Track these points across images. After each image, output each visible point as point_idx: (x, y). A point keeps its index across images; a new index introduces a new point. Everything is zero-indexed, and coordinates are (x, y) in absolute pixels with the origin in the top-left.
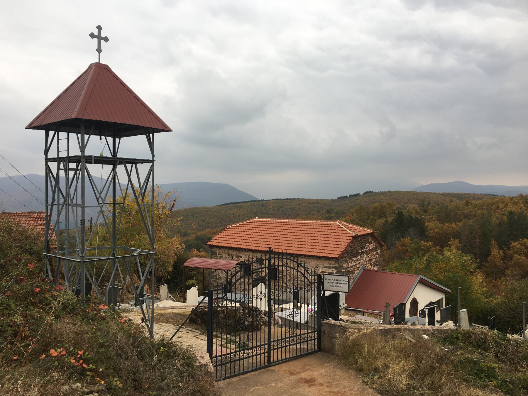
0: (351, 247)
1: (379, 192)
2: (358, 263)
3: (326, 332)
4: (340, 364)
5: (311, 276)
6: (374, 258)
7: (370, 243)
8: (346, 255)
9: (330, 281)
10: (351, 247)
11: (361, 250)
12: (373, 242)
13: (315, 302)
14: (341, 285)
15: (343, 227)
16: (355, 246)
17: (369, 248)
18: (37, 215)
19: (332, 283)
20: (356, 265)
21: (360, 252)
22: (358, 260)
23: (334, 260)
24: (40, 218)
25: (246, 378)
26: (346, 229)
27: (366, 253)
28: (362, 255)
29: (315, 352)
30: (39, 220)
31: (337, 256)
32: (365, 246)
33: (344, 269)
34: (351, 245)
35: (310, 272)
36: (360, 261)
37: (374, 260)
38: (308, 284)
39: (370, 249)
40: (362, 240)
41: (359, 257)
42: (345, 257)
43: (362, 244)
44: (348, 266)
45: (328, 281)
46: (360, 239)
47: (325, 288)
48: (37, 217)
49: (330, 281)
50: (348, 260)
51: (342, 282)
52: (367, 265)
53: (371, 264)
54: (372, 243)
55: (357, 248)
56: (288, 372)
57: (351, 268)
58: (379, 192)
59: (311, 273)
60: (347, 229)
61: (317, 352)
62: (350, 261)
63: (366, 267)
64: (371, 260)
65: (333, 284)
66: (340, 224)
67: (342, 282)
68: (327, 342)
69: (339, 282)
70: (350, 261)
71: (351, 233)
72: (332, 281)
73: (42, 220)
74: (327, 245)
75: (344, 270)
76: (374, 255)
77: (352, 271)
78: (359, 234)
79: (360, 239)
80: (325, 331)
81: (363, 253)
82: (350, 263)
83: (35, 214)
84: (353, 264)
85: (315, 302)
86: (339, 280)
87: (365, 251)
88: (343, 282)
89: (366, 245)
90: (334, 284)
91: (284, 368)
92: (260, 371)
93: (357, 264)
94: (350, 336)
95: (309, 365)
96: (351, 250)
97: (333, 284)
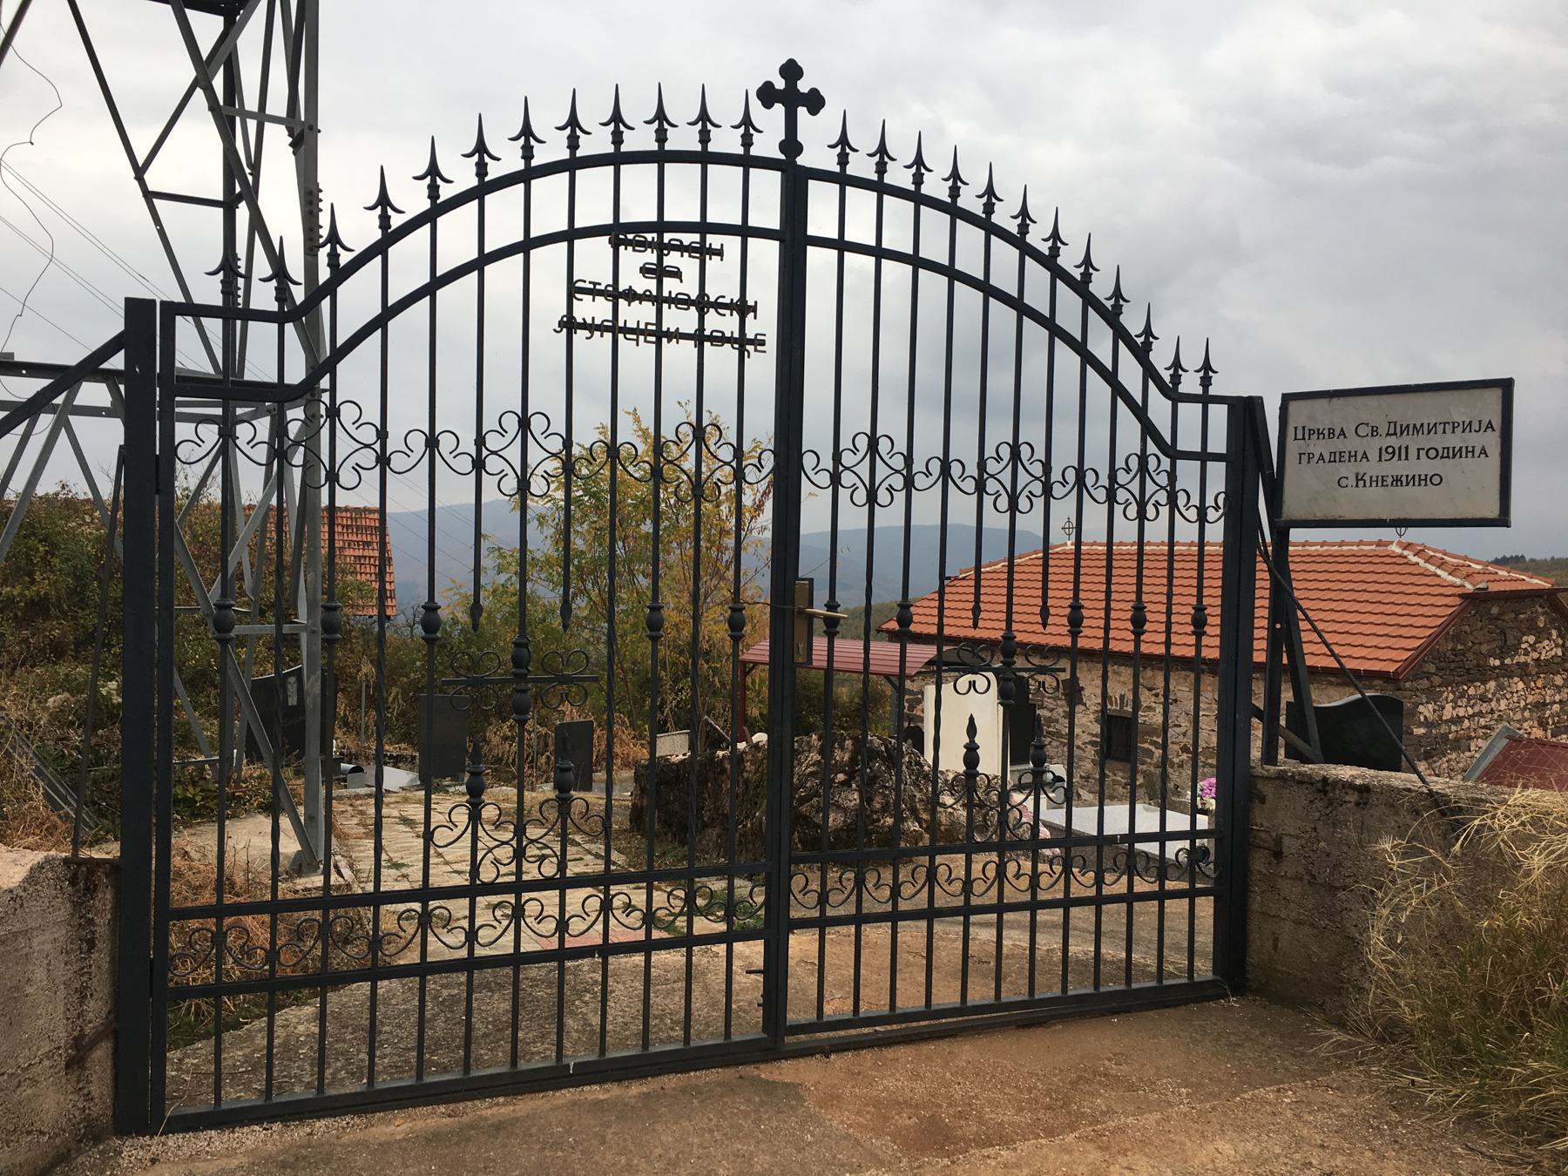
0: (1457, 638)
1: (1549, 559)
2: (1485, 708)
3: (1290, 845)
4: (1405, 1101)
5: (1171, 393)
6: (1557, 698)
7: (1541, 634)
8: (1432, 668)
9: (1338, 444)
10: (1457, 638)
11: (1502, 659)
12: (1554, 633)
13: (1200, 609)
14: (1426, 467)
15: (1421, 562)
16: (1471, 638)
17: (1535, 655)
18: (351, 518)
19: (1353, 456)
20: (1473, 715)
21: (1495, 668)
22: (1483, 699)
23: (1376, 682)
24: (357, 527)
25: (499, 1127)
26: (1432, 568)
27: (1523, 672)
28: (1505, 681)
29: (1187, 995)
30: (352, 533)
31: (1392, 668)
32: (1520, 642)
33: (1420, 725)
34: (1452, 630)
35: (1161, 358)
36: (1493, 704)
37: (1556, 707)
38: (1143, 458)
39: (1538, 659)
40: (1506, 618)
41: (1492, 685)
42: (1428, 676)
43: (1503, 632)
44: (1440, 717)
45: (1318, 447)
46: (1495, 610)
47: (1293, 506)
48: (349, 523)
49: (1338, 444)
50: (1441, 693)
51: (1439, 441)
52: (1526, 725)
53: (1543, 724)
54: (1551, 634)
55: (1484, 648)
56: (904, 1120)
57: (1454, 728)
58: (1549, 559)
59: (1176, 379)
60: (1439, 567)
61: (1216, 998)
62: (1451, 697)
63: (1521, 732)
64: (1545, 704)
65: (1363, 467)
66: (1406, 553)
67: (1439, 441)
68: (1298, 923)
69: (1413, 442)
70: (1451, 697)
71: (1458, 581)
72: (1352, 444)
73: (362, 534)
74: (1347, 627)
75: (1422, 731)
76: (1557, 686)
77: (1457, 740)
78: (1494, 587)
79: (1495, 610)
80: (1278, 841)
81: (1506, 671)
82: (1449, 707)
83: (344, 514)
84: (1461, 712)
85: (1200, 609)
86: (1417, 429)
87: (1518, 664)
88: (1455, 440)
89: (1524, 638)
90: (1372, 468)
91: (890, 1083)
92: (671, 1081)
93: (1480, 714)
94: (1522, 840)
95: (1111, 1081)
96: (1453, 650)
97: (1363, 467)
